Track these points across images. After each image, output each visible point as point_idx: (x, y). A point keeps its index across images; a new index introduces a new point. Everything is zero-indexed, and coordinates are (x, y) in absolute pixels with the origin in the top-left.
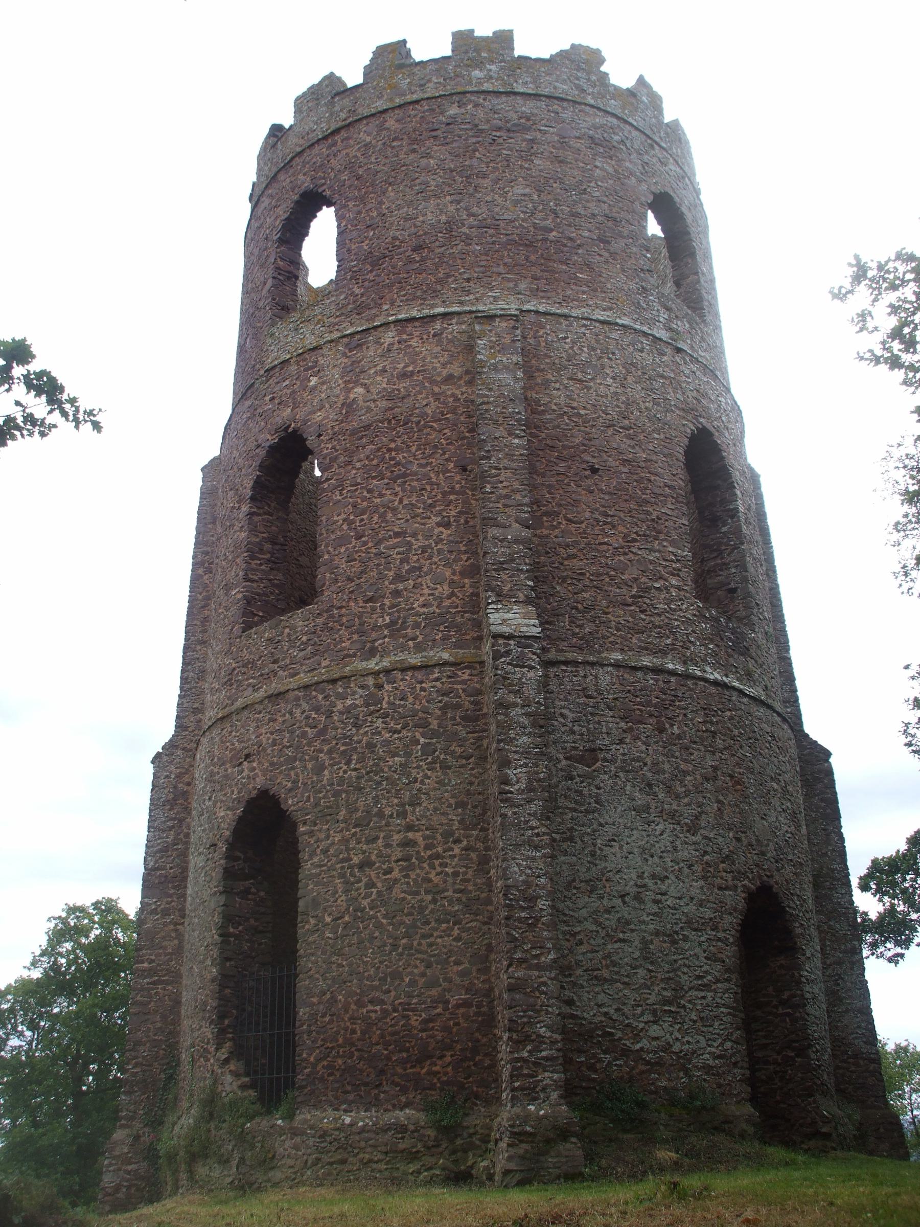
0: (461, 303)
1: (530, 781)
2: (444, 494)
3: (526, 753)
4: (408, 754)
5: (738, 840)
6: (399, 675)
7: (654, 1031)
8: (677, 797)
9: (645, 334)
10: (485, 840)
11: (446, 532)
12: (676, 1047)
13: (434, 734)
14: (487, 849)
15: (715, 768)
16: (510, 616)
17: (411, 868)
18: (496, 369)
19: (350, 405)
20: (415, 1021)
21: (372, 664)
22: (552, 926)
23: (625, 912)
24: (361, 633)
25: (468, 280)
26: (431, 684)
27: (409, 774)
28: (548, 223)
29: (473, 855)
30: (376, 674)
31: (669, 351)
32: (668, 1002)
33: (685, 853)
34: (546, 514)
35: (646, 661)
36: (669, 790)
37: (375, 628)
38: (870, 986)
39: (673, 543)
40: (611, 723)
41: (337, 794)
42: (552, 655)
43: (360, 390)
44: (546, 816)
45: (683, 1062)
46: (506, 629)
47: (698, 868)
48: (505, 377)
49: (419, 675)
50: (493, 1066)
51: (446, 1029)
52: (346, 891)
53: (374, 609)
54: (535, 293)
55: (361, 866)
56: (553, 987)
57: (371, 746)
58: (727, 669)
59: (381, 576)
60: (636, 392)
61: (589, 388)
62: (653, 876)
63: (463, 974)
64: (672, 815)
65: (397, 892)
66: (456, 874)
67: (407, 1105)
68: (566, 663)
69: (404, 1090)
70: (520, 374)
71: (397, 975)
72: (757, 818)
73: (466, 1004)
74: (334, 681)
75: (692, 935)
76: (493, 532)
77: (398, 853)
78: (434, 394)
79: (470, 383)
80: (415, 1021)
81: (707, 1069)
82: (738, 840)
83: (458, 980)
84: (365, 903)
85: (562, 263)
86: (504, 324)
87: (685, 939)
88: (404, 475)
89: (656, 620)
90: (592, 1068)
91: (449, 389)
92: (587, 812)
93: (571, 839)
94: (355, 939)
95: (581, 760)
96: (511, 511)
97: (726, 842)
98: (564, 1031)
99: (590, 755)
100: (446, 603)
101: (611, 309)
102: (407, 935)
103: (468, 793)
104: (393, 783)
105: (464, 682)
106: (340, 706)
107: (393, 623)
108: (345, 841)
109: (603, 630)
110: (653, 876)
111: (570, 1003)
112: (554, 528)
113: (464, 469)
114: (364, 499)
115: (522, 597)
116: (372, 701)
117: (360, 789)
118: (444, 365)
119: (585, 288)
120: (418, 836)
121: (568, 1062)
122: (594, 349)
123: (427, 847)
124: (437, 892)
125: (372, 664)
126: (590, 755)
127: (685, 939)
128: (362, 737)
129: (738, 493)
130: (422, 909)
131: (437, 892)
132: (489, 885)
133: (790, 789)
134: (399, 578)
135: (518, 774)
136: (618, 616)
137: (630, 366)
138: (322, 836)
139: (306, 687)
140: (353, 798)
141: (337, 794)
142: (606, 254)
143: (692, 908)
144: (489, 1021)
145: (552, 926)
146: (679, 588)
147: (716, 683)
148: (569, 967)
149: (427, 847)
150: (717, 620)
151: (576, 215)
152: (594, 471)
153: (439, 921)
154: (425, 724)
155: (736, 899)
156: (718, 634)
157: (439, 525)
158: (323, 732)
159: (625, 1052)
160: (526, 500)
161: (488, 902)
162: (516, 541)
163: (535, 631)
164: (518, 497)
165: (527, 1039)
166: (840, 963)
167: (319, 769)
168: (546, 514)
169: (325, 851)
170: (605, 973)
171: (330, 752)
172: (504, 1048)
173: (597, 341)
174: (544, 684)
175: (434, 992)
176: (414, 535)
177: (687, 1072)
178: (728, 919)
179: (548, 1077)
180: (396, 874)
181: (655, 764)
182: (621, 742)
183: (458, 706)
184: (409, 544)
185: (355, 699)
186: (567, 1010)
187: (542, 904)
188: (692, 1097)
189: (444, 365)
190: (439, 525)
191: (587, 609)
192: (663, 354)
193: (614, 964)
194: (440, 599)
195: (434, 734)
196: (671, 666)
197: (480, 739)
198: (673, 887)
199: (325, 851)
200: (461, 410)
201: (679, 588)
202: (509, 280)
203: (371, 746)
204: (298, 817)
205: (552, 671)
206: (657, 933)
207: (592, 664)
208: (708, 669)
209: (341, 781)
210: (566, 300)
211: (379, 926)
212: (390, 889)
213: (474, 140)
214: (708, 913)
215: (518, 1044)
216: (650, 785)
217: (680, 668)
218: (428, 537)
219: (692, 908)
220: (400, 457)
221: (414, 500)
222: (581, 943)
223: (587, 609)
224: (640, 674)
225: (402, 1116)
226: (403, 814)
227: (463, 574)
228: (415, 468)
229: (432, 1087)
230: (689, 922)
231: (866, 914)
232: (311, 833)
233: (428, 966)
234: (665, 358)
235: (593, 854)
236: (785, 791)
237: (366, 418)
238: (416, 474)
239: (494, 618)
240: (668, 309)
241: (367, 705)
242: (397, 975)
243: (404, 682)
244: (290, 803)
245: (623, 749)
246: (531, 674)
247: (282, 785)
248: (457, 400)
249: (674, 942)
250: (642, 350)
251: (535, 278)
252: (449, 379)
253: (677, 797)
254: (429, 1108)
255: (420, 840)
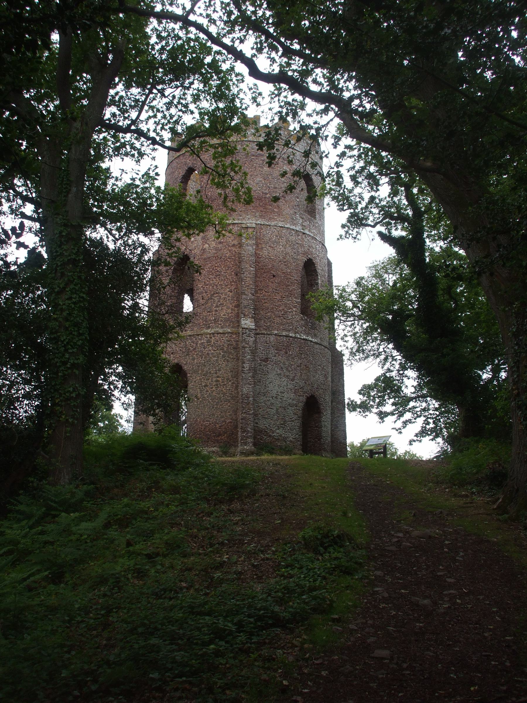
0: (238, 219)
1: (249, 368)
2: (231, 282)
3: (249, 360)
4: (218, 357)
5: (305, 383)
6: (216, 335)
7: (278, 431)
8: (289, 371)
9: (293, 230)
10: (237, 381)
11: (231, 294)
12: (283, 436)
13: (225, 352)
14: (238, 383)
15: (301, 363)
16: (247, 322)
17: (218, 387)
18: (248, 245)
19: (204, 250)
20: (217, 426)
21: (209, 331)
22: (253, 404)
23: (273, 401)
24: (206, 321)
25: (241, 211)
26: (225, 338)
27: (218, 363)
28: (267, 191)
29: (234, 385)
30: (210, 334)
31: (301, 234)
32: (282, 424)
33: (290, 386)
34: (259, 290)
35: (284, 334)
36: (287, 369)
37: (210, 320)
38: (347, 424)
39: (296, 298)
40: (273, 351)
41: (198, 366)
42: (258, 331)
43: (207, 245)
44: (253, 377)
45: (285, 439)
46: (246, 326)
47: (293, 390)
48: (250, 248)
49: (222, 335)
50: (237, 438)
51: (225, 428)
52: (201, 393)
53: (210, 315)
54: (261, 216)
55: (205, 386)
56: (252, 419)
57: (208, 354)
58: (308, 334)
59: (212, 305)
60: (289, 250)
61: (275, 249)
62: (281, 392)
63: (230, 415)
64: (287, 376)
65: (214, 393)
66: (229, 390)
67: (215, 447)
68: (262, 334)
69: (214, 443)
70: (254, 247)
71: (213, 415)
72: (312, 377)
73: (231, 422)
74: (198, 335)
75: (290, 408)
76: (244, 296)
77: (215, 383)
78: (229, 250)
79: (240, 247)
80: (217, 426)
81: (291, 441)
82: (305, 383)
83: (229, 416)
84: (206, 396)
85: (270, 205)
86: (251, 230)
87: (288, 409)
88: (220, 275)
89: (288, 321)
90: (261, 439)
91: (233, 249)
92: (264, 375)
93: (260, 382)
94: (203, 405)
95: (264, 361)
96: (249, 290)
97: (302, 384)
98: (254, 430)
99: (266, 360)
100: (230, 315)
101: (284, 221)
102: (216, 405)
103: (234, 368)
104: (214, 365)
105: (234, 338)
106: (200, 342)
107: (215, 319)
108: (200, 379)
109: (273, 324)
110: (281, 392)
111: (257, 423)
112: (261, 294)
113: (237, 275)
114: (208, 281)
115: (251, 316)
116: (209, 341)
117: (205, 366)
118: (232, 241)
119: (276, 214)
120: (220, 379)
121: (255, 438)
122: (277, 236)
123: (222, 382)
124: (224, 394)
125: (209, 331)
126: (266, 360)
127: (288, 409)
128: (206, 351)
129: (319, 277)
130: (220, 398)
131: (224, 394)
132: (238, 393)
133: (325, 368)
134: (217, 306)
135: (247, 366)
136: (277, 320)
137: (288, 241)
138: (194, 377)
139: (190, 336)
140: (203, 368)
141: (198, 366)
142: (284, 202)
143: (291, 401)
144: (236, 427)
145: (253, 404)
146: (296, 311)
147: (304, 339)
148: (257, 414)
149: (222, 382)
150: (306, 320)
151: (275, 188)
152: (274, 276)
153: (225, 401)
154: (223, 349)
155: (304, 399)
156: (306, 324)
157: (229, 291)
158: (195, 349)
159: (270, 436)
160: (254, 287)
161: (237, 397)
162: (250, 300)
163: (254, 327)
164: (251, 286)
165: (245, 431)
166: (339, 417)
167: (194, 359)
168: (259, 290)
169: (195, 382)
170: (266, 416)
171: (197, 355)
172: (239, 433)
173: (278, 233)
174: (255, 342)
175: (223, 419)
176: (222, 294)
177: (285, 442)
178: (300, 404)
179: (250, 440)
180: (214, 389)
181: (284, 362)
182: (275, 356)
183: (232, 345)
184: (220, 296)
185: (204, 341)
186: (256, 425)
187: (251, 399)
188: (286, 448)
189: (232, 241)
190: (229, 291)
191: (269, 318)
192: (298, 236)
193: (269, 414)
194: (228, 314)
195: (225, 352)
196: (291, 335)
197: (237, 354)
198: (286, 395)
199: (195, 382)
200: (237, 256)
201: (296, 311)
202: (253, 212)
203: (208, 354)
204: (188, 372)
205: (258, 336)
206: (281, 407)
207: (269, 334)
208: (302, 335)
209: (200, 363)
210: (270, 219)
211: (209, 402)
212: (212, 392)
213: (245, 159)
214: (295, 402)
215: (243, 432)
216: (282, 368)
217: (293, 335)
218: (226, 295)
219: (291, 401)
220: (218, 269)
221: (222, 283)
222: (260, 408)
223: (269, 318)
224: (282, 337)
225: (214, 449)
226: (216, 373)
227: (235, 307)
228: (223, 273)
229: (221, 442)
230: (289, 404)
231: (356, 402)
232: (191, 376)
233: (222, 413)
234: (299, 237)
235: (265, 386)
236: (323, 368)
237: (209, 255)
238: (222, 275)
239: (243, 322)
240: (303, 218)
241: (207, 343)
242: (213, 415)
243: (218, 337)
244: (185, 368)
245: (275, 358)
246: (252, 339)
247: (183, 362)
248: (236, 252)
249: (285, 409)
250: (292, 236)
251: (261, 211)
252: (234, 245)
253: (289, 371)
254: (220, 447)
255: (221, 380)
